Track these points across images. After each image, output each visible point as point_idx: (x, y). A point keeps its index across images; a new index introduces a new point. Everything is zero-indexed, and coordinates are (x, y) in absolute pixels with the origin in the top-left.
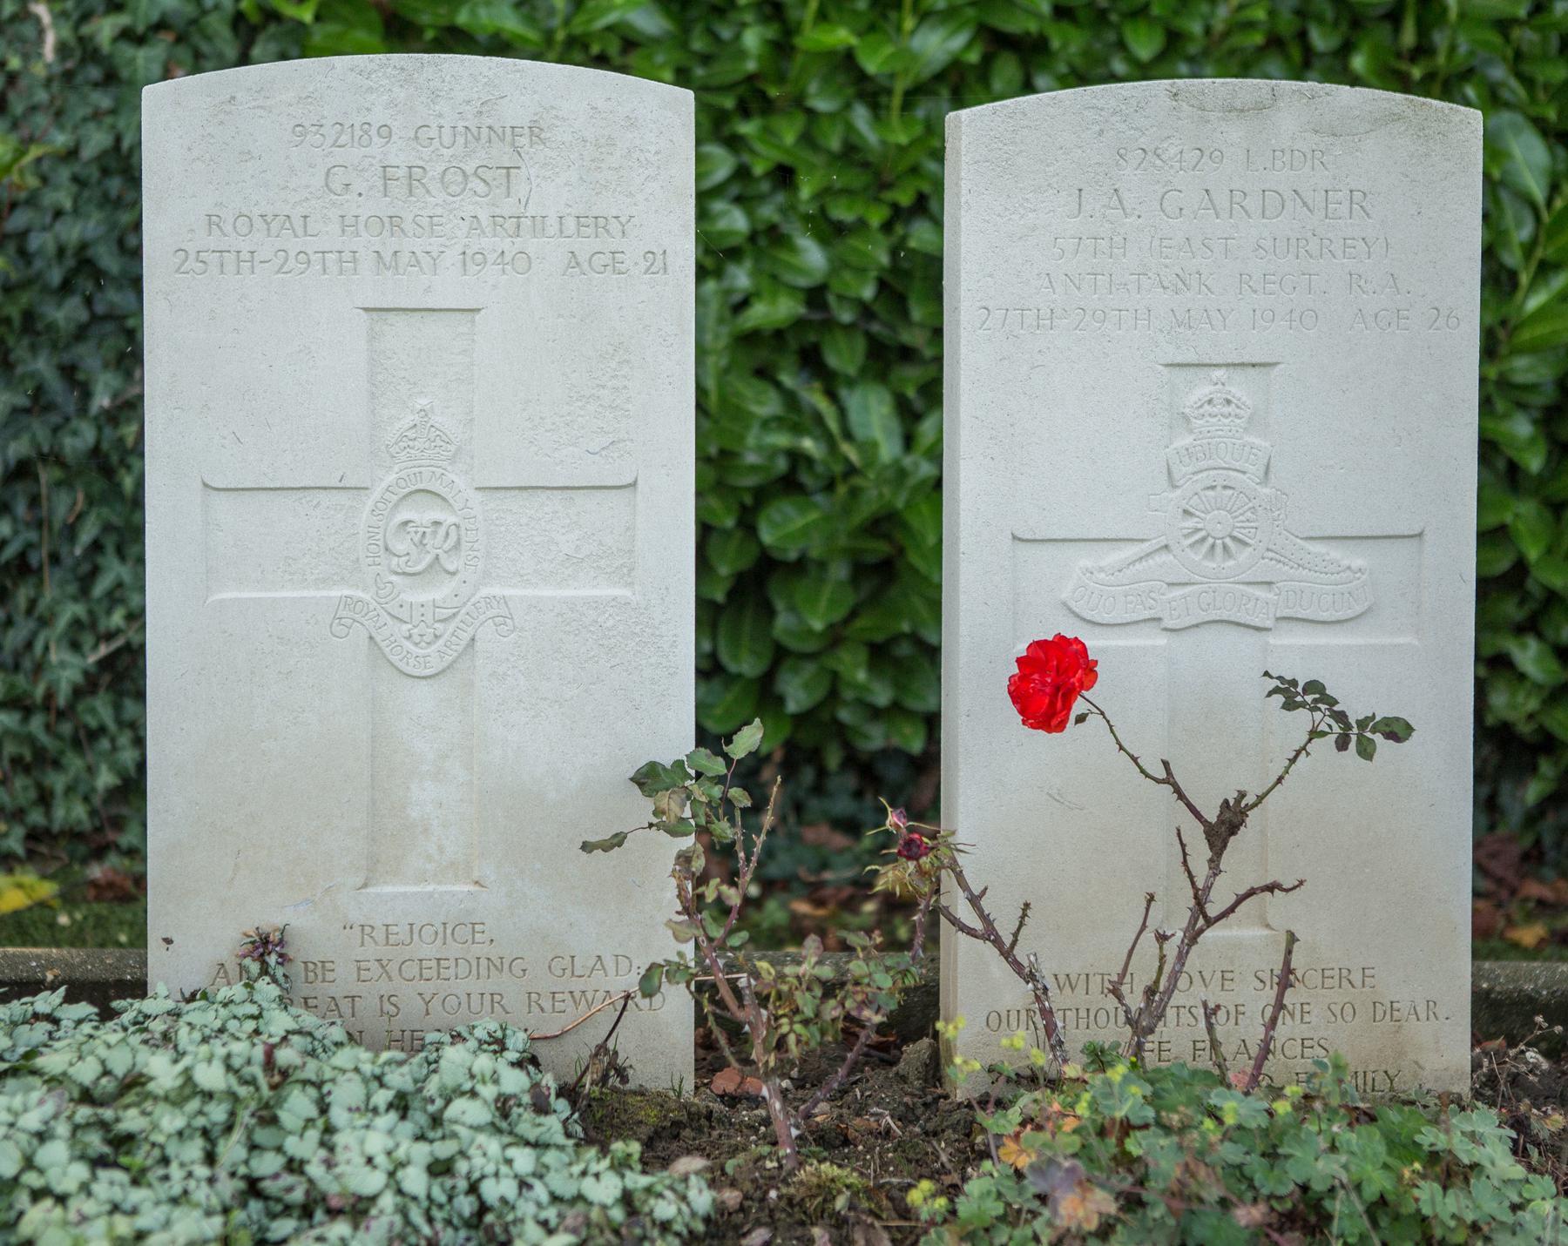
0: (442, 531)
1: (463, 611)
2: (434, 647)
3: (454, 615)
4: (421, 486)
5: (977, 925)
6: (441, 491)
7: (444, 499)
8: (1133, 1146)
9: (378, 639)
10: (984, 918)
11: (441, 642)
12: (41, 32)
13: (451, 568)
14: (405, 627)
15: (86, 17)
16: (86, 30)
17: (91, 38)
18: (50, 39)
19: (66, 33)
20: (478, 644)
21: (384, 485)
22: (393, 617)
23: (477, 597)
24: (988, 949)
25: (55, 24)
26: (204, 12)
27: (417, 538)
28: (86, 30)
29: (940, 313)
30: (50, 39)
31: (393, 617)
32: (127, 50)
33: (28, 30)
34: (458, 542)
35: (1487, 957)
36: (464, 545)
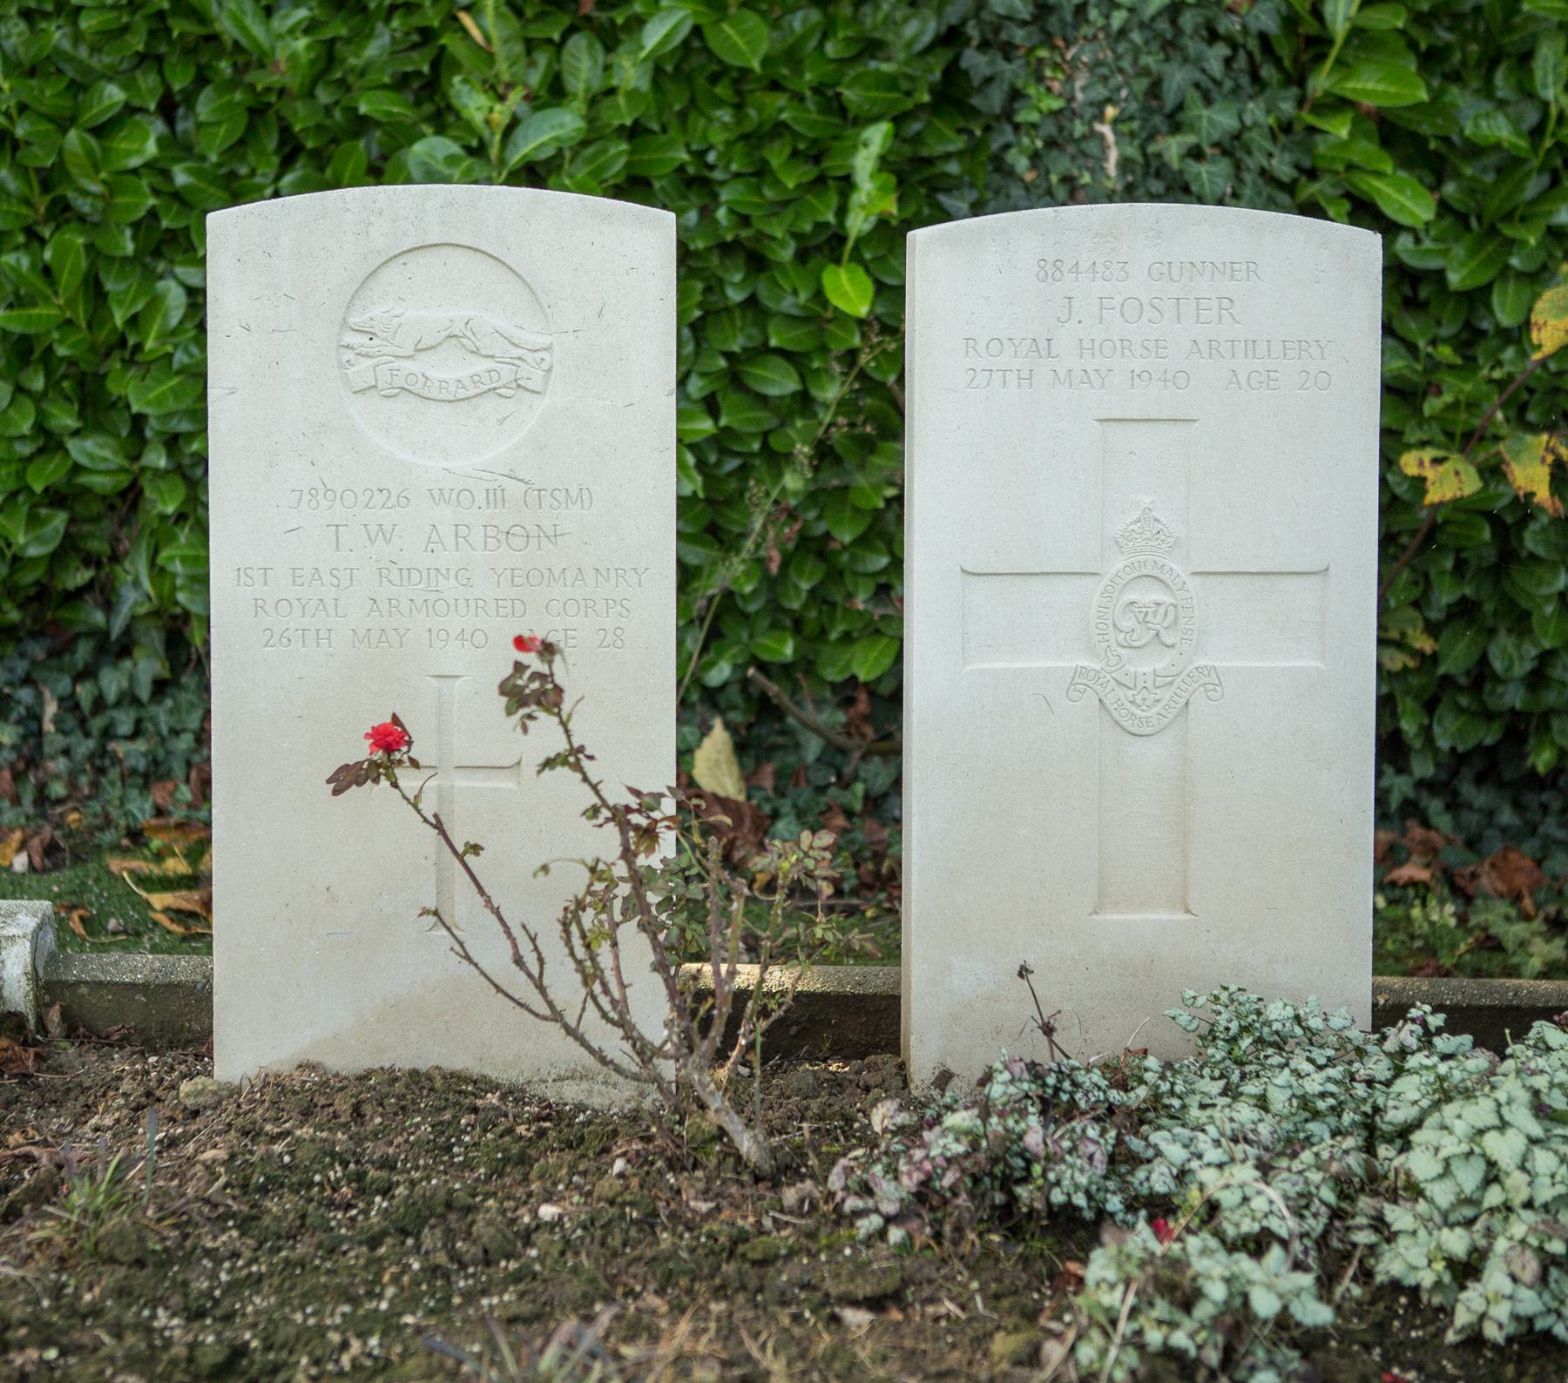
0: (1162, 610)
1: (1178, 680)
2: (1153, 711)
3: (1171, 683)
4: (1145, 572)
5: (546, 1011)
6: (1162, 577)
7: (1168, 586)
8: (734, 1176)
9: (1106, 702)
10: (550, 1004)
11: (1160, 705)
12: (1104, 148)
13: (1169, 642)
14: (1130, 693)
15: (1151, 137)
16: (1152, 148)
17: (1159, 155)
18: (1113, 156)
19: (1132, 151)
20: (1191, 707)
21: (1113, 571)
22: (1119, 683)
23: (1191, 668)
24: (554, 1028)
25: (1117, 143)
26: (1244, 128)
27: (1141, 617)
28: (1152, 148)
29: (203, 396)
30: (1113, 156)
31: (1119, 683)
32: (1193, 167)
33: (1092, 147)
34: (1176, 619)
35: (1381, 974)
36: (1182, 621)
